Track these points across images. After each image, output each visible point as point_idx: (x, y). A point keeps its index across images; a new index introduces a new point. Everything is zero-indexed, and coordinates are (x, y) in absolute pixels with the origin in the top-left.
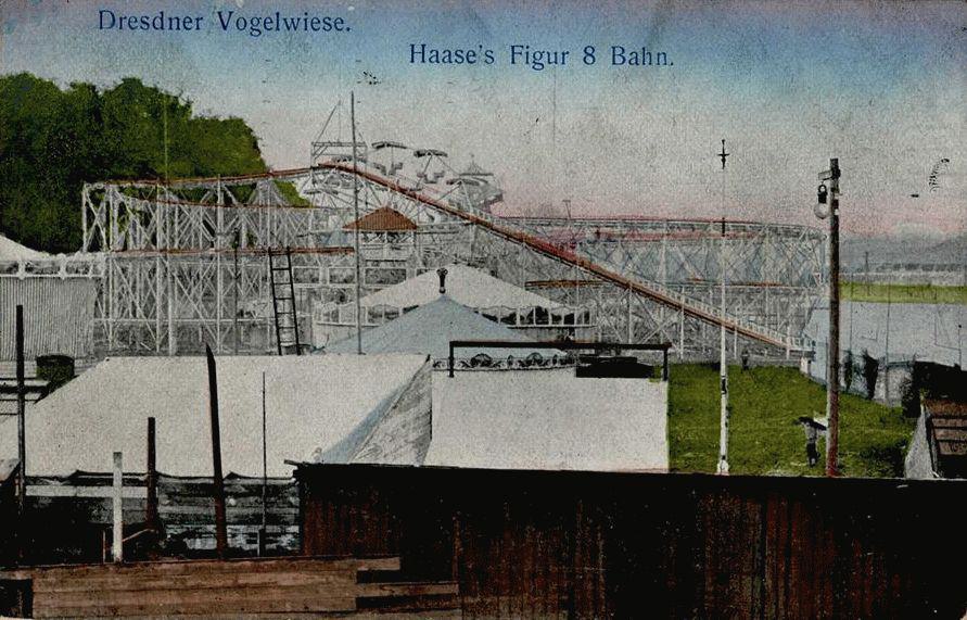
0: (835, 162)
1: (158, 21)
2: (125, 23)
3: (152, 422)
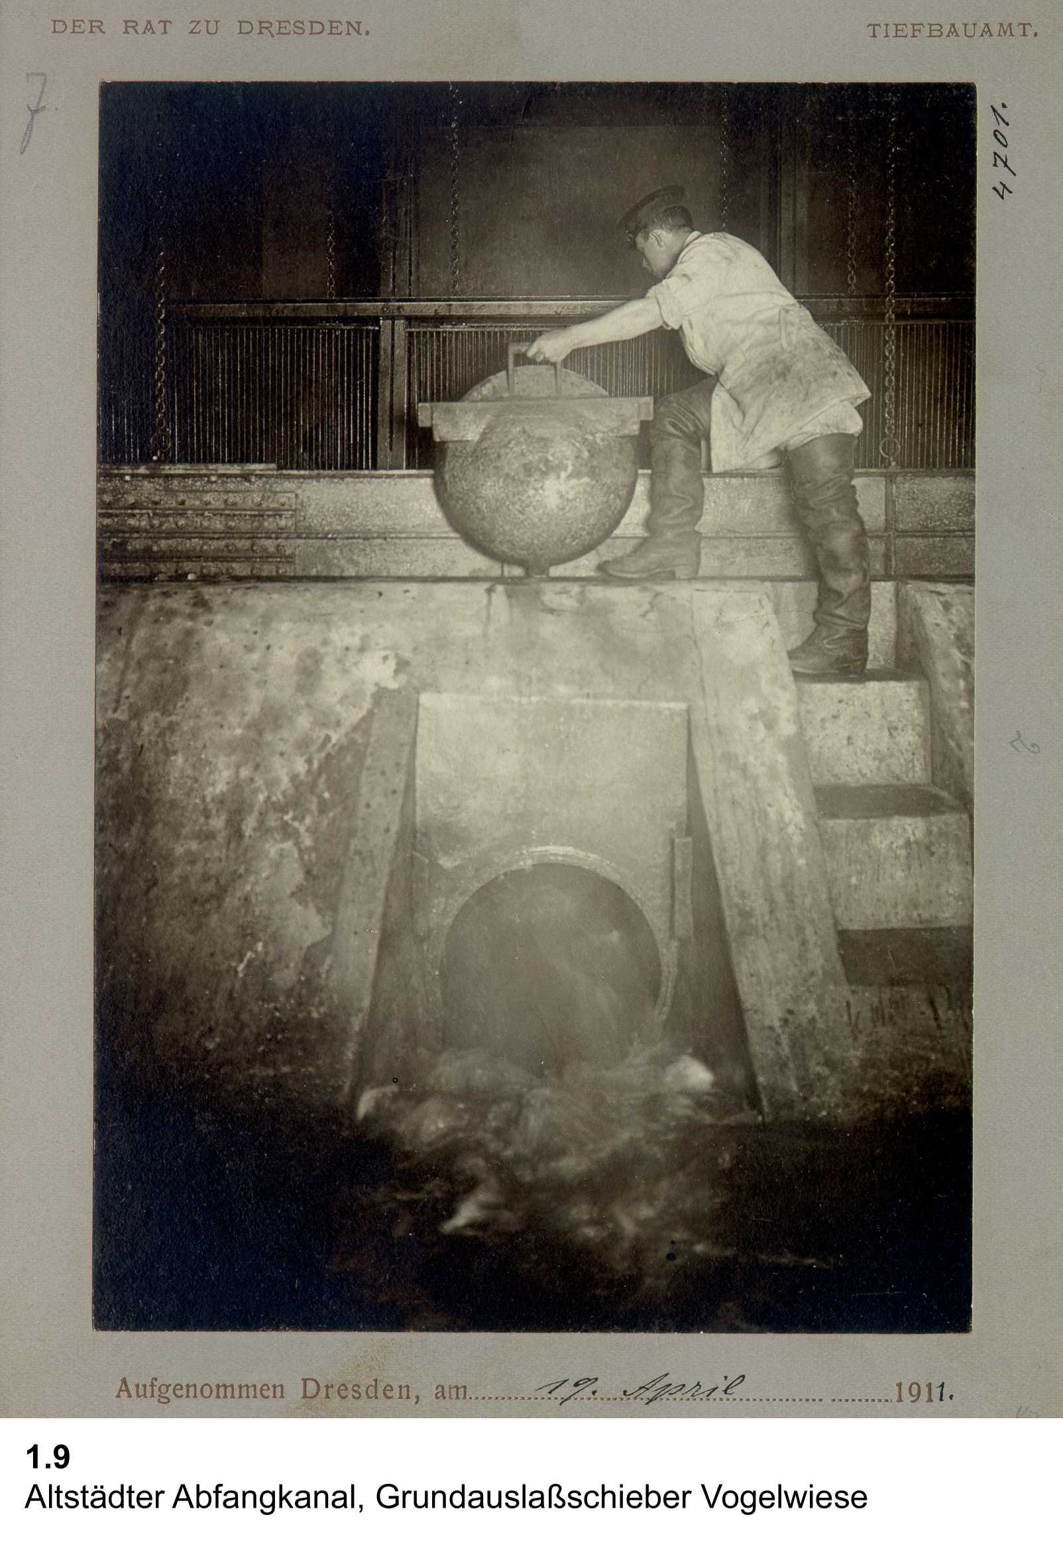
3: (858, 1499)
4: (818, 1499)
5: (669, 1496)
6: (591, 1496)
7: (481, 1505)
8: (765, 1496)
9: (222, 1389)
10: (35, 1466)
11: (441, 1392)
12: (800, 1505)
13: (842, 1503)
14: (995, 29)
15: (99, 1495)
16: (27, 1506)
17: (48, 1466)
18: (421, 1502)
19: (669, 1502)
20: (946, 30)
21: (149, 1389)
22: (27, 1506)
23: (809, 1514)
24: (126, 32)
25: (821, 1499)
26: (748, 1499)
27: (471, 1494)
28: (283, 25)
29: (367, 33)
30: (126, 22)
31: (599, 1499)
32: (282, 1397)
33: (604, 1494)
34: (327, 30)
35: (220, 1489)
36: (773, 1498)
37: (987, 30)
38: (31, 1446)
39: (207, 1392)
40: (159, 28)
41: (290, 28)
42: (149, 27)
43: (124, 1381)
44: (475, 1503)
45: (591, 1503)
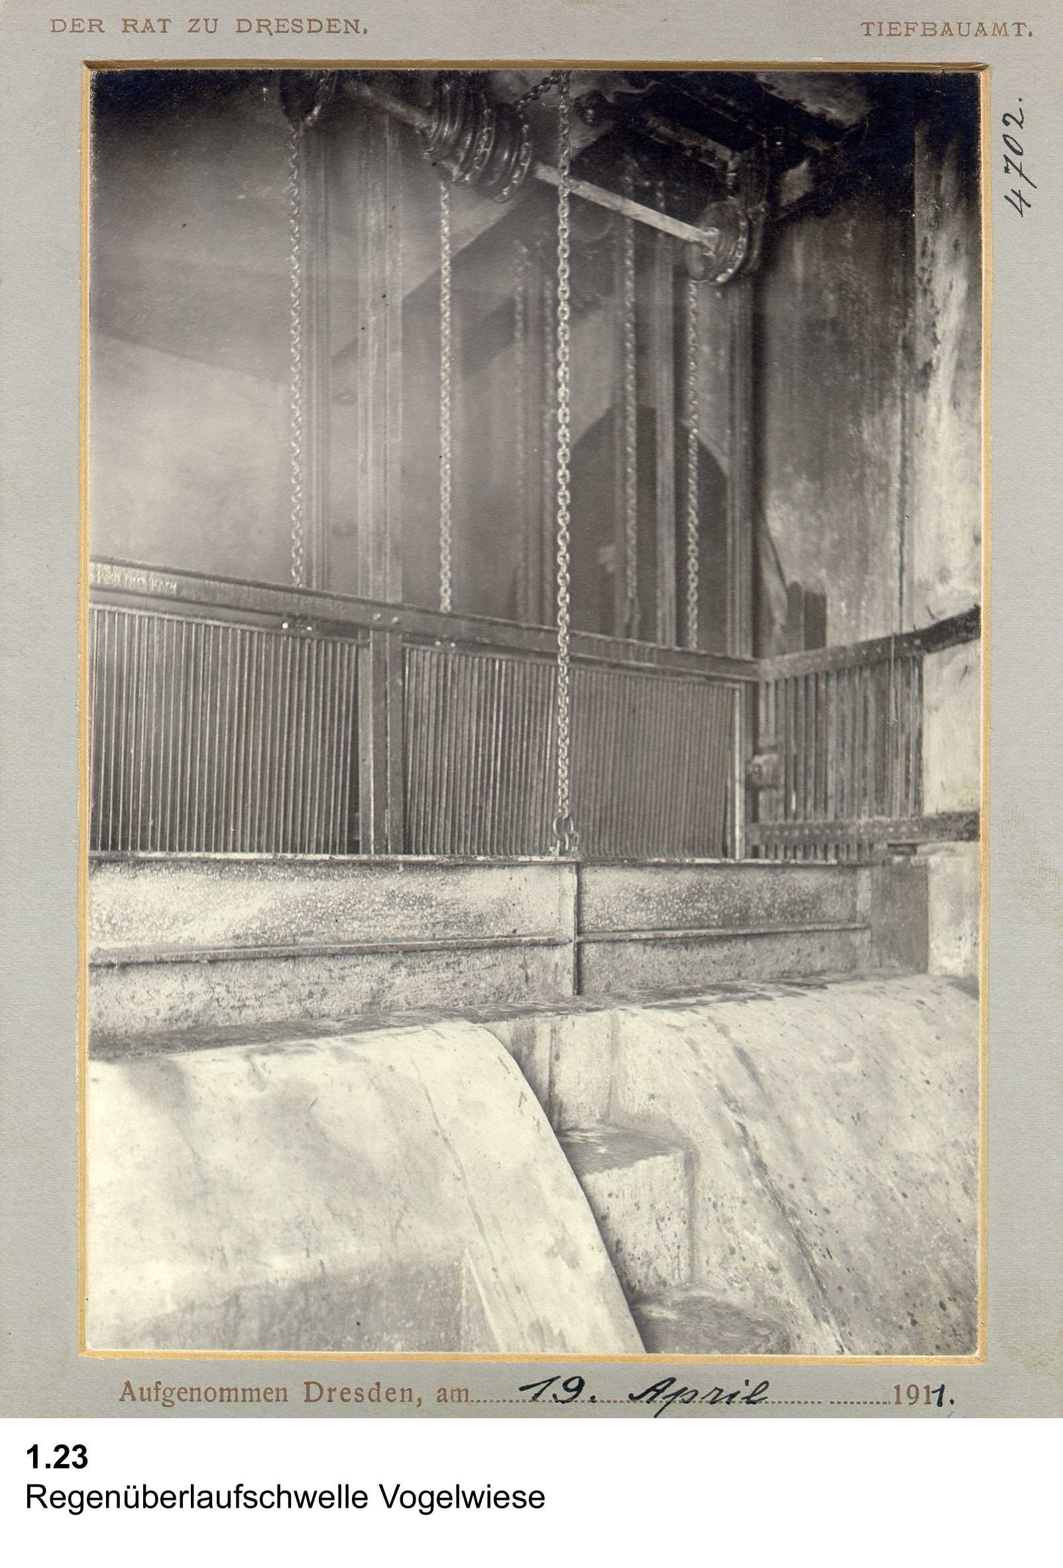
0: (943, 1386)
1: (374, 1395)
2: (336, 1396)
3: (535, 1499)
5: (166, 1496)
6: (267, 1496)
7: (210, 1505)
9: (456, 1393)
10: (35, 1466)
12: (478, 1505)
13: (520, 1503)
14: (989, 27)
16: (29, 1506)
17: (48, 1466)
19: (166, 1502)
20: (940, 29)
21: (153, 1392)
22: (29, 1506)
23: (486, 1514)
24: (126, 31)
25: (498, 1499)
26: (426, 1499)
27: (200, 1494)
29: (365, 31)
30: (125, 21)
31: (275, 1499)
32: (285, 1400)
33: (279, 1494)
34: (326, 28)
35: (241, 1489)
36: (333, 1498)
38: (31, 1446)
40: (158, 27)
41: (288, 26)
44: (204, 1503)
45: (267, 1503)
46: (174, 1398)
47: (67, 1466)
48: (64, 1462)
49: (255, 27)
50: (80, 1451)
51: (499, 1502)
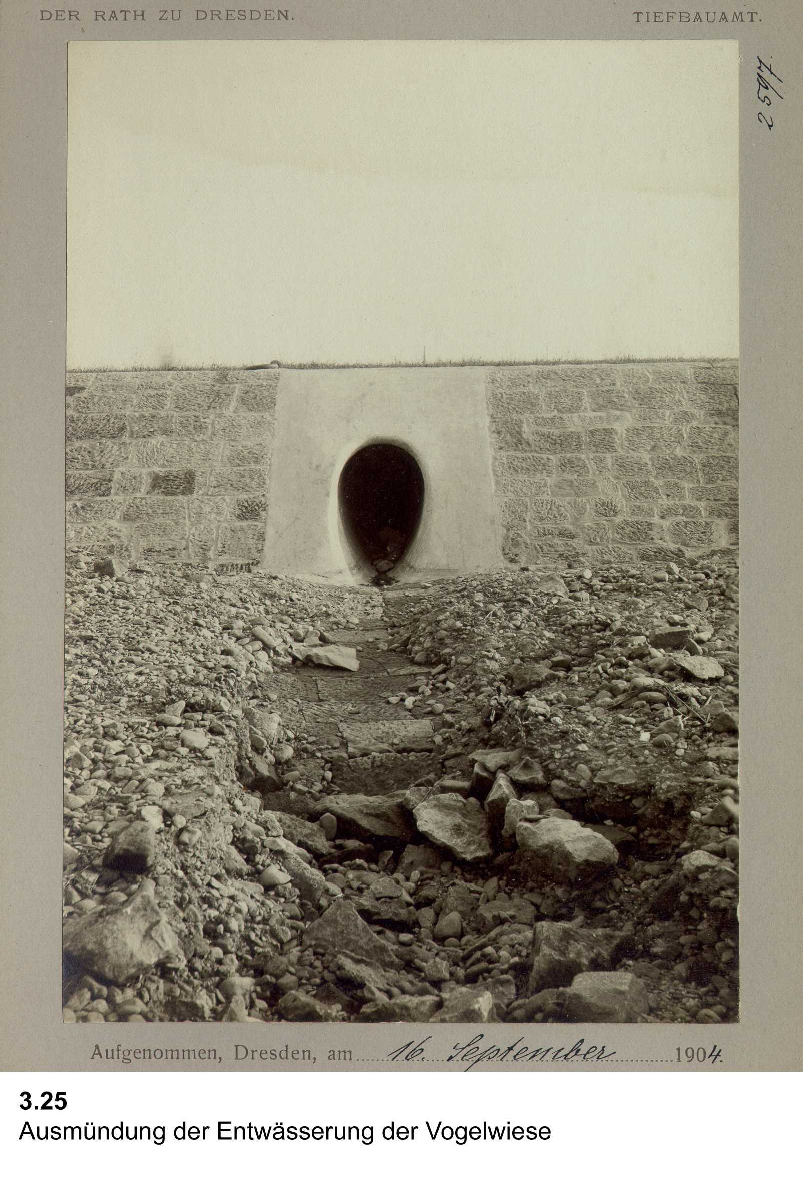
1: (284, 1054)
2: (257, 1055)
3: (544, 1133)
4: (514, 1133)
8: (401, 1130)
11: (332, 1056)
12: (500, 1138)
13: (532, 1136)
15: (280, 1130)
16: (20, 1138)
17: (36, 1108)
18: (340, 1135)
20: (692, 17)
21: (115, 1053)
22: (20, 1138)
23: (507, 1144)
25: (516, 1133)
26: (461, 1133)
28: (59, 13)
34: (54, 17)
36: (480, 1132)
37: (724, 17)
39: (158, 1054)
40: (120, 16)
42: (113, 15)
43: (97, 1047)
44: (278, 1136)
46: (131, 1056)
47: (51, 1108)
48: (48, 1105)
49: (209, 16)
50: (25, 1096)
51: (473, 1135)
